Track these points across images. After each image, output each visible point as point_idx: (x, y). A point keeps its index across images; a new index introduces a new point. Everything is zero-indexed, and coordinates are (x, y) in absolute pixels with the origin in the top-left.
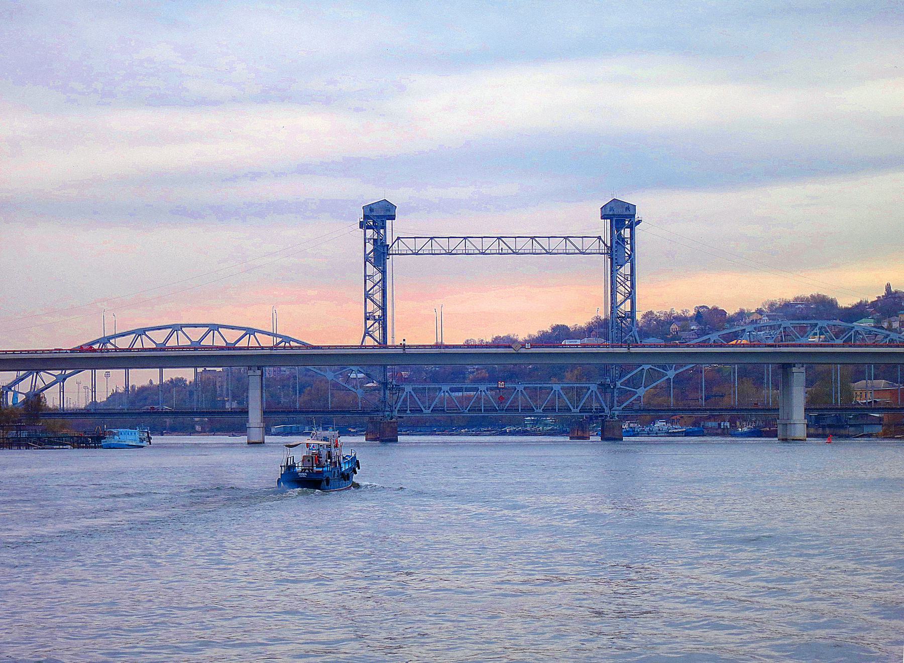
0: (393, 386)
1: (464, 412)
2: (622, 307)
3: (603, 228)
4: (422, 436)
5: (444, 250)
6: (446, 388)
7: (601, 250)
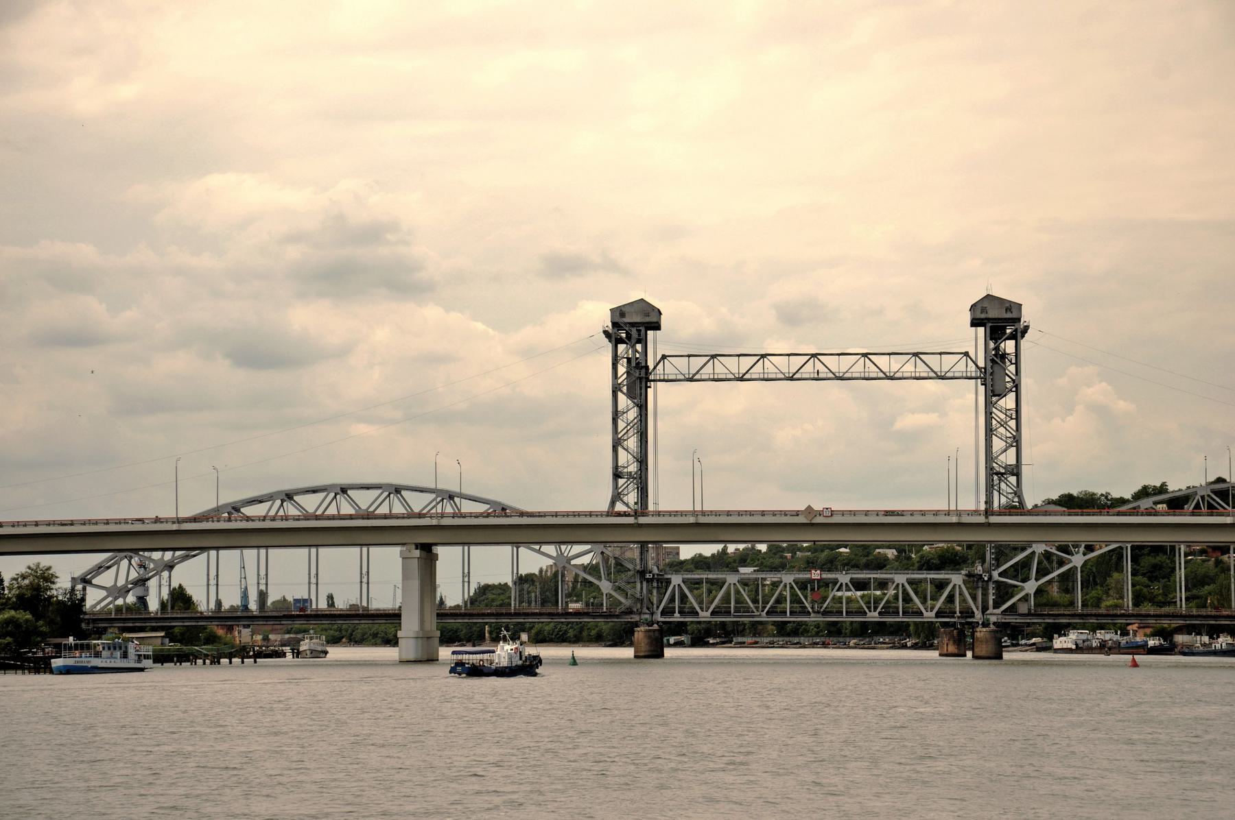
0: (653, 575)
1: (760, 615)
2: (1002, 458)
3: (974, 341)
4: (1014, 653)
5: (782, 372)
6: (844, 578)
7: (658, 376)
